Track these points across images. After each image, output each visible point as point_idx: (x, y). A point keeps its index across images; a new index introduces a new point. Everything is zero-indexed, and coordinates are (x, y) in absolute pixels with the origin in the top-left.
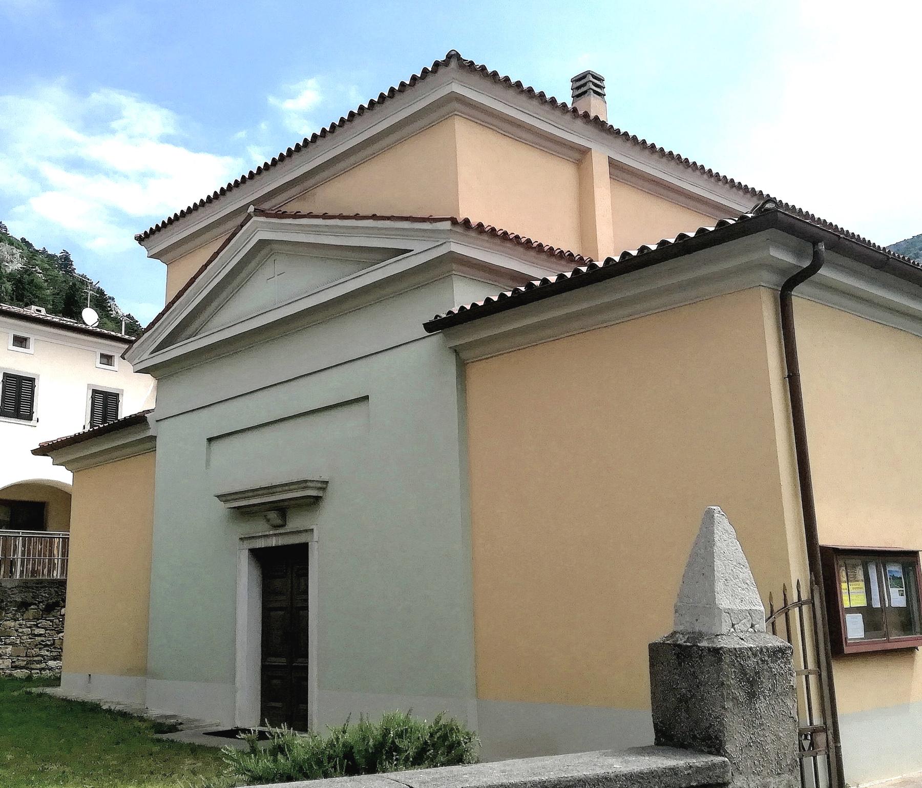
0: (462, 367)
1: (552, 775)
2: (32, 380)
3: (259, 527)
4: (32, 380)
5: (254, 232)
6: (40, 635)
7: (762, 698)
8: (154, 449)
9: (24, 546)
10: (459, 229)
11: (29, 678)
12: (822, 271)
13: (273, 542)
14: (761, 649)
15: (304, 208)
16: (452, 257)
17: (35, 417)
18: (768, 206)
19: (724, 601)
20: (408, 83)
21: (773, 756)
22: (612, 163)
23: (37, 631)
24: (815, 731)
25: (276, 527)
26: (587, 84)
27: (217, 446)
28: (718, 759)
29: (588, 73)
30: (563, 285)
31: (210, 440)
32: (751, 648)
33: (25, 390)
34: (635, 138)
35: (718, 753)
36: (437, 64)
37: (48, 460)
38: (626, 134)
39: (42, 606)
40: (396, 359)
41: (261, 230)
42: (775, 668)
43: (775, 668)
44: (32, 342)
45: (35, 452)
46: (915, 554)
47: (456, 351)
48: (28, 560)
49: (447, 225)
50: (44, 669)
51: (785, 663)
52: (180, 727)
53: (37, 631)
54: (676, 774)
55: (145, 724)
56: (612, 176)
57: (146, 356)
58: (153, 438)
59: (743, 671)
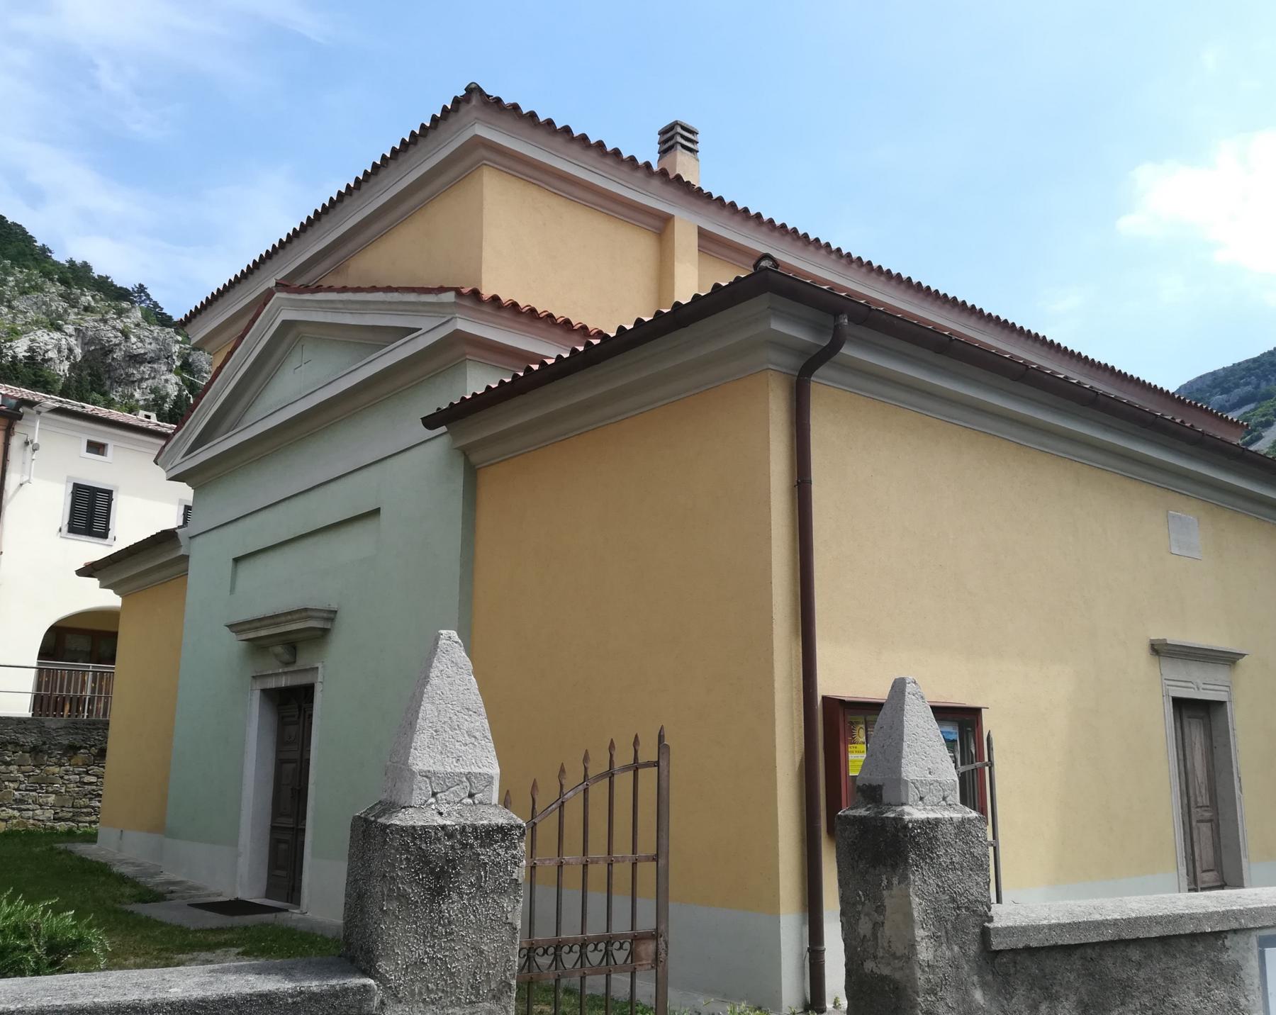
0: (472, 475)
1: (104, 998)
2: (110, 493)
3: (271, 665)
4: (110, 493)
5: (278, 311)
6: (91, 783)
7: (455, 896)
8: (185, 573)
9: (94, 681)
10: (467, 303)
11: (70, 833)
12: (846, 350)
13: (283, 682)
14: (464, 828)
15: (338, 282)
16: (458, 338)
17: (111, 535)
18: (764, 264)
19: (423, 758)
20: (428, 124)
21: (464, 980)
22: (702, 234)
23: (87, 779)
24: (636, 939)
25: (287, 664)
26: (675, 137)
27: (244, 568)
28: (357, 981)
29: (676, 124)
30: (563, 369)
31: (237, 560)
32: (444, 827)
33: (101, 502)
34: (733, 205)
35: (365, 973)
36: (456, 101)
37: (95, 582)
38: (720, 199)
39: (94, 750)
40: (404, 466)
41: (285, 309)
42: (486, 854)
43: (486, 854)
44: (110, 450)
45: (80, 573)
46: (975, 713)
47: (465, 452)
48: (99, 698)
49: (450, 297)
50: (95, 822)
51: (507, 848)
52: (169, 896)
53: (87, 779)
54: (271, 1003)
55: (127, 891)
56: (701, 249)
57: (178, 460)
58: (185, 558)
59: (424, 858)
